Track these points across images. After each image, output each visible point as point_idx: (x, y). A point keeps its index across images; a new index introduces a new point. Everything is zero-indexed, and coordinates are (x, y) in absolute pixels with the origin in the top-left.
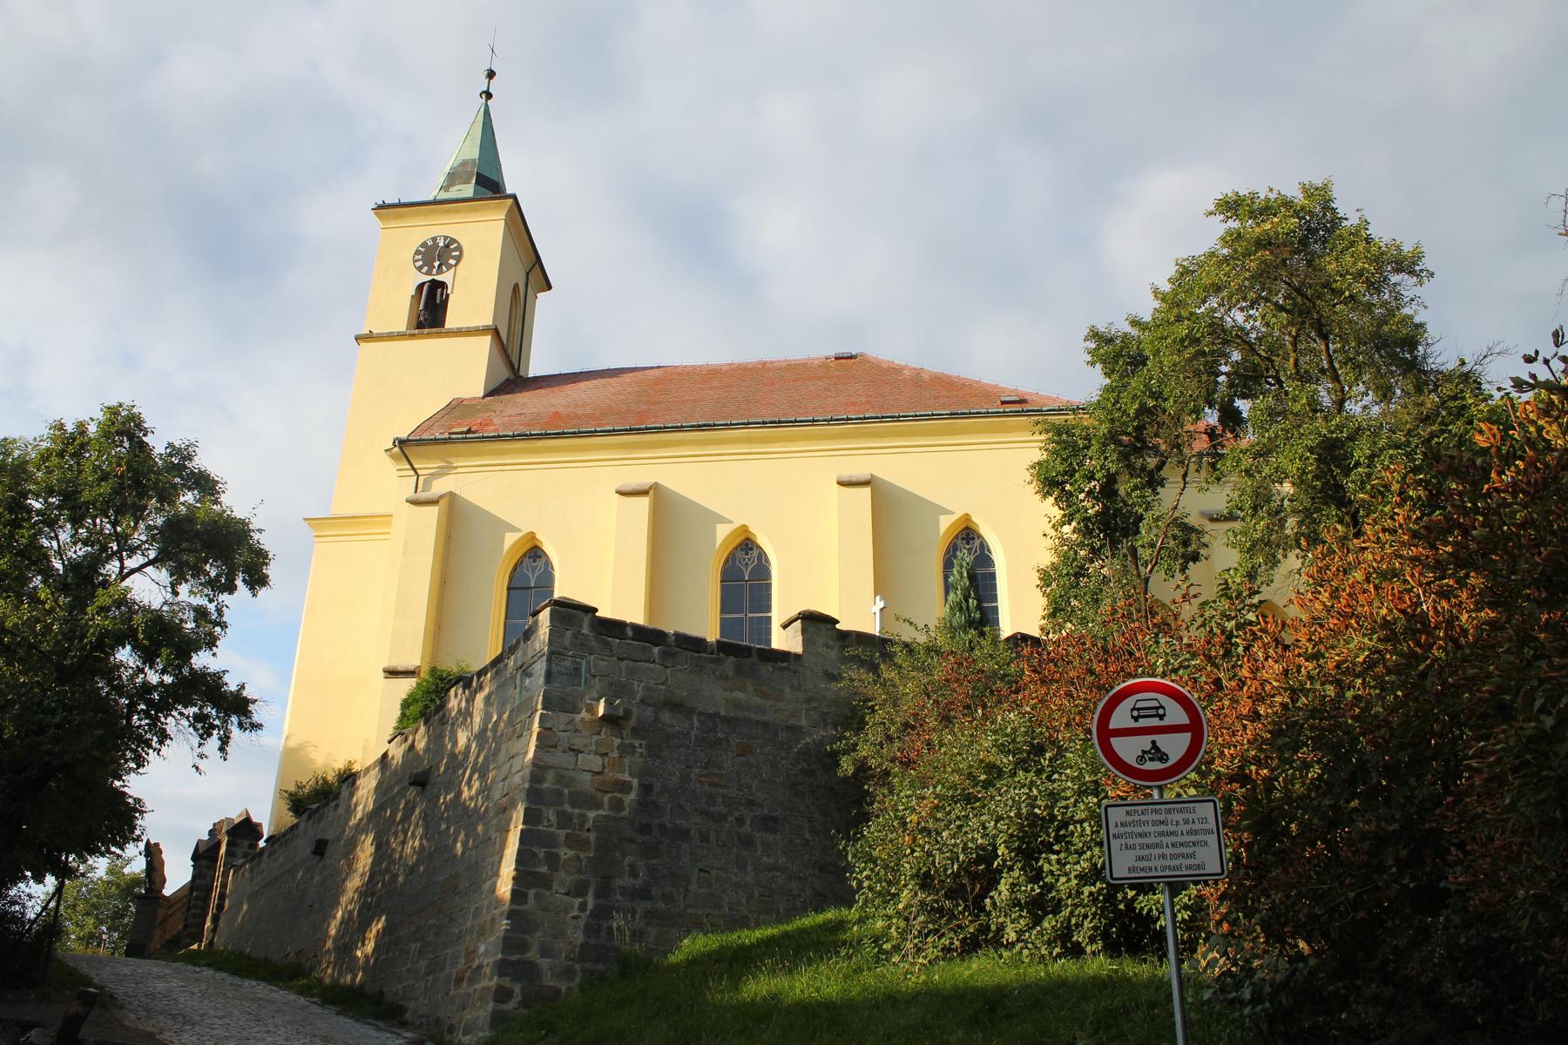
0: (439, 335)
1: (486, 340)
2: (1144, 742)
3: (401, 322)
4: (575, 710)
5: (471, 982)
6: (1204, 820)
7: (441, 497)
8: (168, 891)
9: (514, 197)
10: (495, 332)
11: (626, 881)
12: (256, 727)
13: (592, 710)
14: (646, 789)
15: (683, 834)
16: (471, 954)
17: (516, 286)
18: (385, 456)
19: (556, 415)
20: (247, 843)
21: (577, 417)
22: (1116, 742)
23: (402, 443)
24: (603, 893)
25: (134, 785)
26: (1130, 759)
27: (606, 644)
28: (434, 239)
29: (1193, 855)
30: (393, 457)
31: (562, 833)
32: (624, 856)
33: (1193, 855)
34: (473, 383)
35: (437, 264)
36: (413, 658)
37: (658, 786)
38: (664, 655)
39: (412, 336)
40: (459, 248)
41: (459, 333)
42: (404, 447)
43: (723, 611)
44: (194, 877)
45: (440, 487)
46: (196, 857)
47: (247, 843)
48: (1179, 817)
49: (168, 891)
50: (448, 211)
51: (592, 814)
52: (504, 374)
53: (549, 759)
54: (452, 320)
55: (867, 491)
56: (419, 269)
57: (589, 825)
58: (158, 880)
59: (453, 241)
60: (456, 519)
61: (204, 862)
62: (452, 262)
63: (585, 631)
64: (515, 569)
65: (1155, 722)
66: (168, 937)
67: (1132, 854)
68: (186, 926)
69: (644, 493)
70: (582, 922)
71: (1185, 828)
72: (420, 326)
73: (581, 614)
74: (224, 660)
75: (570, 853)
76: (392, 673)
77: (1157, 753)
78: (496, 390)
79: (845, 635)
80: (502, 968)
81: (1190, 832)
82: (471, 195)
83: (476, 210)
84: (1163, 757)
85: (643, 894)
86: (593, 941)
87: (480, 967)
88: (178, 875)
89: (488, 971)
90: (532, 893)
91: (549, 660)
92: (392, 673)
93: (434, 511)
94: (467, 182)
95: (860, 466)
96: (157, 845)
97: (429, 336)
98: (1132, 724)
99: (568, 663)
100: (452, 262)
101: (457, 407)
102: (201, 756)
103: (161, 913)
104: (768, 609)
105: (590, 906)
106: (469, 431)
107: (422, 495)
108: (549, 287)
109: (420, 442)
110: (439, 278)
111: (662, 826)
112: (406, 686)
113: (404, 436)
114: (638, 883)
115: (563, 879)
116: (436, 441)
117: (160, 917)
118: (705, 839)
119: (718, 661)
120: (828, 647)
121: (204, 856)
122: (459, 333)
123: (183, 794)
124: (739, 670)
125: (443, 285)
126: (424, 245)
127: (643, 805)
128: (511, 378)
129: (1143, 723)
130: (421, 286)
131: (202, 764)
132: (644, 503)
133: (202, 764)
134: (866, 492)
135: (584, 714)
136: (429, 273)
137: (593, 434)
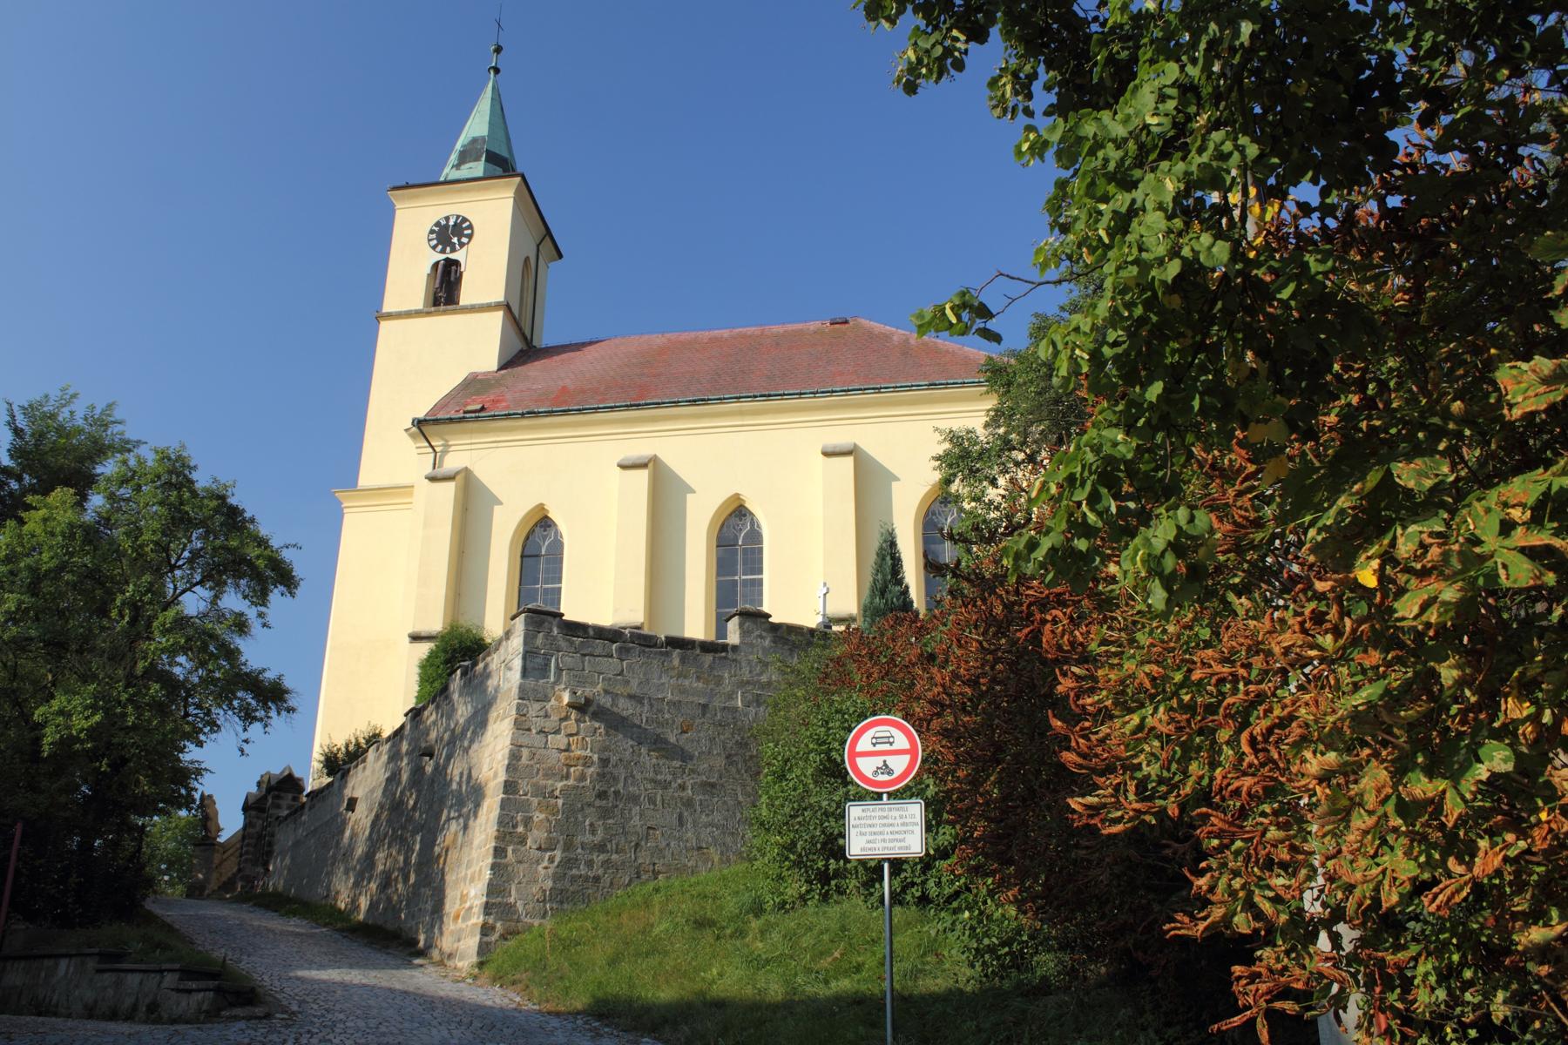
0: (455, 312)
1: (500, 314)
2: (878, 761)
3: (418, 302)
4: (546, 699)
5: (464, 920)
6: (913, 816)
7: (457, 473)
8: (223, 838)
9: (523, 177)
10: (507, 307)
11: (588, 838)
12: (290, 710)
13: (559, 699)
14: (604, 762)
15: (634, 799)
16: (464, 898)
17: (527, 260)
18: (405, 435)
19: (564, 389)
20: (290, 796)
21: (583, 391)
22: (860, 761)
23: (419, 423)
24: (568, 847)
25: (191, 754)
26: (868, 773)
27: (572, 643)
28: (447, 219)
29: (903, 840)
30: (412, 436)
31: (535, 801)
32: (585, 817)
33: (903, 840)
34: (487, 358)
35: (455, 240)
36: (436, 625)
37: (614, 759)
38: (620, 650)
39: (428, 314)
40: (471, 227)
41: (473, 309)
42: (422, 426)
43: (718, 574)
44: (245, 828)
45: (452, 463)
46: (246, 808)
47: (290, 796)
48: (897, 814)
49: (223, 838)
50: (460, 191)
51: (560, 785)
52: (518, 345)
53: (524, 740)
54: (466, 296)
55: (849, 460)
56: (434, 248)
57: (557, 793)
58: (213, 829)
59: (465, 220)
60: (472, 502)
61: (253, 813)
62: (464, 240)
63: (555, 631)
64: (527, 538)
65: (887, 747)
66: (224, 879)
67: (865, 838)
68: (239, 870)
69: (644, 466)
70: (550, 871)
71: (899, 821)
72: (436, 303)
73: (550, 619)
74: (256, 653)
75: (542, 816)
76: (416, 638)
77: (886, 769)
78: (509, 362)
79: (776, 628)
80: (487, 908)
81: (903, 824)
82: (480, 174)
83: (486, 189)
84: (890, 772)
85: (601, 848)
86: (559, 886)
87: (471, 908)
88: (230, 822)
89: (475, 910)
90: (510, 849)
91: (524, 659)
92: (416, 638)
93: (450, 487)
94: (477, 159)
95: (842, 435)
96: (210, 797)
97: (445, 312)
98: (872, 748)
99: (539, 660)
100: (464, 240)
101: (473, 384)
102: (246, 741)
103: (217, 858)
104: (760, 571)
105: (557, 860)
106: (483, 409)
107: (439, 472)
108: (560, 256)
109: (437, 421)
110: (453, 256)
111: (617, 793)
112: (424, 649)
113: (421, 415)
114: (598, 838)
115: (537, 836)
116: (451, 420)
117: (216, 861)
118: (652, 801)
119: (667, 654)
120: (761, 637)
121: (252, 807)
122: (473, 309)
123: (228, 769)
124: (683, 660)
125: (457, 263)
126: (438, 224)
127: (602, 776)
128: (523, 349)
129: (879, 747)
130: (437, 264)
131: (245, 746)
132: (643, 476)
133: (245, 746)
134: (849, 462)
135: (553, 702)
136: (443, 251)
137: (596, 410)
